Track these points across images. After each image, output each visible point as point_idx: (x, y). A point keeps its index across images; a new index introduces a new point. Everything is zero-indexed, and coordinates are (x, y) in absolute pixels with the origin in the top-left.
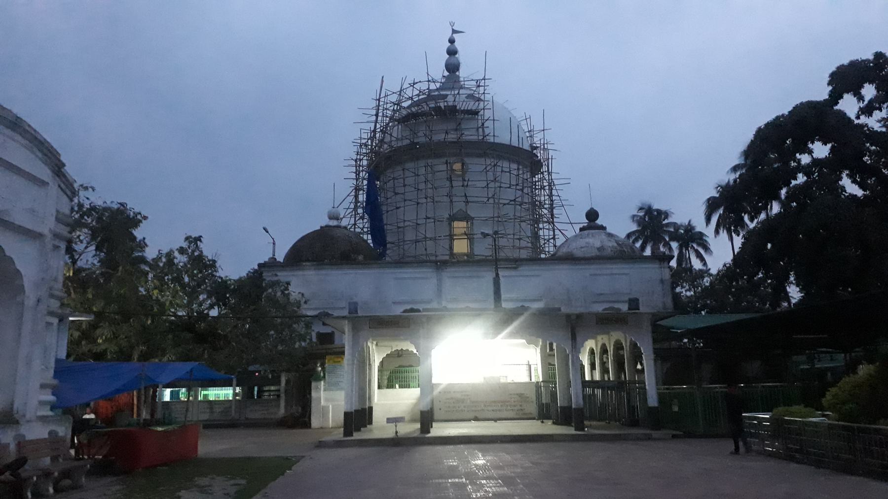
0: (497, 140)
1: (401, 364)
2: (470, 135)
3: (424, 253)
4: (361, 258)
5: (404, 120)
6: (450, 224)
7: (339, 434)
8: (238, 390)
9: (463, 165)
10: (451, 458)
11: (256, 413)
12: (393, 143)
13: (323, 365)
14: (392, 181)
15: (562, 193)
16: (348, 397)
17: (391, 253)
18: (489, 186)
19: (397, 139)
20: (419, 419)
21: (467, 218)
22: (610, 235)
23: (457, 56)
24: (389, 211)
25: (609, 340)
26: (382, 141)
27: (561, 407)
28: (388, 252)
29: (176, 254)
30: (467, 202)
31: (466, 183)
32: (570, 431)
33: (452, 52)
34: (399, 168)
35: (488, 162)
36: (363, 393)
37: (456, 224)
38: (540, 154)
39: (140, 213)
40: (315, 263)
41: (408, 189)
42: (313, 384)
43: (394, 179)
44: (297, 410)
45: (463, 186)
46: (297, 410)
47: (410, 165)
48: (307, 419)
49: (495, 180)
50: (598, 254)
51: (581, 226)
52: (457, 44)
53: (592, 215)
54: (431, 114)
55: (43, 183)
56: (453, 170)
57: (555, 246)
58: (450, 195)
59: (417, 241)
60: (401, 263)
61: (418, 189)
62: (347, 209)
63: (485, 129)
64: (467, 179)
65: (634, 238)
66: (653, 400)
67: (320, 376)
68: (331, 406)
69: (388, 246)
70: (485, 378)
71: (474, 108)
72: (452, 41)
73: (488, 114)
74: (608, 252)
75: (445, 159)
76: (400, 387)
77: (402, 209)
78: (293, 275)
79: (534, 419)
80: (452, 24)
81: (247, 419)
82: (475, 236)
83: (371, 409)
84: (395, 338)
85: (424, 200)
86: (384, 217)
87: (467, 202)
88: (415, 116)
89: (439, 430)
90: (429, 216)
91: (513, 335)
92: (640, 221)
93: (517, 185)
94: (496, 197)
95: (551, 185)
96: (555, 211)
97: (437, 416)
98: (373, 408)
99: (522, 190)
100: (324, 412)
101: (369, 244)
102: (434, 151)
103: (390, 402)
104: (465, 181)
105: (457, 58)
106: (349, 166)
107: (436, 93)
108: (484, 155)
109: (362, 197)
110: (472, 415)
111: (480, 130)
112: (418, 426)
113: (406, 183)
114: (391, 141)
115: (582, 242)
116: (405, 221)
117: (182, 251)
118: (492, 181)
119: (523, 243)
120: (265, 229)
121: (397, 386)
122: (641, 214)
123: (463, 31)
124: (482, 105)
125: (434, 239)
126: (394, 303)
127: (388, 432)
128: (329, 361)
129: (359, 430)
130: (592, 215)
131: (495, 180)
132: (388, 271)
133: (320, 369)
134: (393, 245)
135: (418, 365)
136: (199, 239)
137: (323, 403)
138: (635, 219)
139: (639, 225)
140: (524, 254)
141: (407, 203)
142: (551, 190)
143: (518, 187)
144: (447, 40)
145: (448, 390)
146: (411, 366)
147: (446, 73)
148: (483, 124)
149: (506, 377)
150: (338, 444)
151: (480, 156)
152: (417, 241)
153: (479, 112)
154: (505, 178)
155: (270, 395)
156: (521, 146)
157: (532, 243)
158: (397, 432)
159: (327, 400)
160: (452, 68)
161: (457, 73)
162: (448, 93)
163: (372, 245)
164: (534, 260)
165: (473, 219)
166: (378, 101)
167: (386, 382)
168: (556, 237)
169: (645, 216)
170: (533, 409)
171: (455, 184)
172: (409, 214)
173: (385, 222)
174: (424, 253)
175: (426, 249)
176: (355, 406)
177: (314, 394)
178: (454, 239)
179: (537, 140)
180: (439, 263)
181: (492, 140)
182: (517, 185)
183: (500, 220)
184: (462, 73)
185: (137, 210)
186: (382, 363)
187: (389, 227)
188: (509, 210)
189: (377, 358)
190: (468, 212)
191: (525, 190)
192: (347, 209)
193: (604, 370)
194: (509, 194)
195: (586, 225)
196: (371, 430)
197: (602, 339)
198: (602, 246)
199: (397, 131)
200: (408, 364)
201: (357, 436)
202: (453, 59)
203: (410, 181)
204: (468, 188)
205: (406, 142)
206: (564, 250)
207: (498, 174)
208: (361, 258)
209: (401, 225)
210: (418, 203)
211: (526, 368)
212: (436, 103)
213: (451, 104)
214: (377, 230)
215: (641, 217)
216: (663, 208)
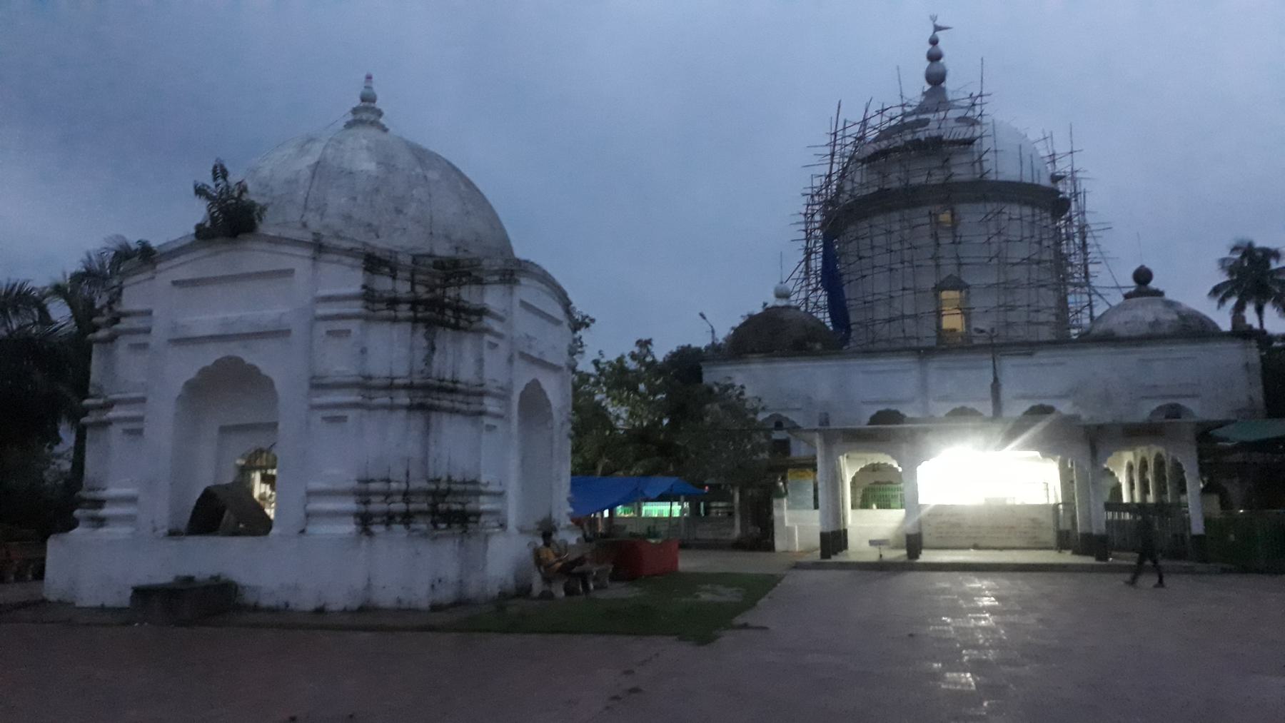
0: (1001, 178)
1: (877, 480)
2: (962, 171)
3: (902, 335)
4: (818, 346)
5: (871, 159)
6: (937, 296)
7: (817, 556)
8: (686, 505)
9: (953, 215)
10: (942, 581)
11: (706, 533)
12: (856, 192)
13: (784, 479)
14: (854, 242)
15: (1100, 243)
16: (824, 520)
17: (857, 335)
18: (991, 241)
19: (861, 185)
20: (905, 544)
21: (958, 285)
22: (1170, 304)
23: (942, 61)
24: (852, 281)
25: (1149, 452)
26: (840, 189)
27: (1082, 534)
28: (853, 334)
29: (628, 359)
30: (960, 265)
31: (958, 240)
32: (1090, 560)
33: (934, 57)
34: (865, 224)
35: (989, 207)
36: (836, 513)
37: (944, 295)
38: (1065, 189)
39: (587, 317)
40: (762, 355)
41: (877, 251)
42: (775, 502)
43: (857, 238)
44: (755, 531)
45: (953, 243)
46: (755, 531)
47: (879, 220)
48: (769, 541)
49: (999, 233)
50: (1150, 331)
51: (1126, 291)
52: (941, 45)
53: (1143, 276)
54: (907, 149)
55: (558, 323)
56: (938, 223)
57: (1092, 317)
58: (935, 258)
59: (890, 320)
60: (869, 352)
61: (892, 251)
62: (798, 279)
63: (985, 164)
64: (958, 234)
65: (1224, 292)
66: (1197, 528)
67: (781, 491)
68: (796, 527)
69: (853, 327)
70: (986, 500)
71: (968, 136)
72: (934, 42)
73: (987, 143)
74: (1165, 329)
75: (929, 208)
76: (878, 508)
77: (870, 277)
78: (737, 370)
79: (1051, 548)
80: (934, 19)
81: (696, 539)
82: (973, 311)
83: (845, 531)
84: (873, 450)
85: (899, 266)
86: (845, 288)
87: (960, 265)
88: (884, 153)
89: (926, 557)
90: (907, 286)
91: (1029, 446)
92: (1232, 268)
93: (1032, 237)
94: (1000, 255)
95: (1083, 229)
96: (1091, 268)
97: (926, 540)
98: (848, 531)
99: (1040, 243)
100: (790, 532)
101: (827, 328)
102: (910, 197)
103: (866, 525)
104: (956, 236)
105: (942, 65)
106: (798, 223)
107: (914, 118)
108: (985, 199)
109: (817, 263)
110: (972, 542)
111: (977, 165)
112: (904, 552)
113: (874, 244)
114: (853, 190)
115: (1124, 316)
116: (874, 294)
117: (633, 356)
118: (995, 235)
119: (1042, 317)
120: (702, 315)
121: (874, 506)
122: (1237, 256)
124: (978, 131)
125: (915, 316)
126: (863, 402)
127: (872, 555)
128: (791, 474)
129: (835, 553)
130: (1143, 276)
131: (999, 233)
132: (852, 362)
133: (781, 484)
134: (858, 326)
135: (901, 481)
136: (649, 342)
137: (787, 524)
138: (1227, 264)
139: (1231, 273)
140: (1045, 334)
141: (876, 270)
142: (1084, 239)
143: (1034, 240)
144: (928, 39)
145: (938, 512)
146: (891, 483)
147: (927, 87)
148: (980, 157)
149: (1014, 498)
150: (815, 566)
151: (977, 200)
152: (890, 320)
153: (974, 141)
154: (1014, 230)
155: (717, 513)
156: (1036, 182)
157: (1057, 316)
158: (881, 556)
159: (791, 520)
160: (936, 79)
161: (943, 85)
162: (930, 116)
163: (831, 328)
164: (1061, 342)
165: (968, 287)
166: (833, 137)
167: (859, 501)
168: (1094, 303)
169: (1242, 257)
170: (1050, 537)
171: (942, 241)
172: (880, 284)
173: (847, 297)
174: (902, 335)
175: (904, 331)
176: (830, 528)
177: (776, 513)
178: (943, 315)
179: (1062, 167)
180: (922, 351)
181: (993, 178)
182: (1032, 237)
183: (1007, 286)
184: (950, 85)
185: (585, 313)
186: (854, 479)
187: (852, 302)
188: (1019, 273)
189: (849, 471)
190: (963, 279)
191: (1045, 243)
192: (798, 279)
193: (1145, 491)
194: (1019, 252)
195: (1133, 289)
196: (847, 555)
197: (1142, 451)
198: (1157, 320)
199: (860, 176)
200: (886, 480)
201: (834, 559)
202: (935, 65)
203: (880, 240)
204: (961, 246)
205: (871, 190)
206: (1100, 328)
207: (1003, 224)
208: (818, 346)
209: (870, 298)
210: (891, 270)
211: (1044, 486)
212: (915, 133)
213: (935, 133)
214: (837, 306)
215: (1236, 262)
216: (1270, 244)
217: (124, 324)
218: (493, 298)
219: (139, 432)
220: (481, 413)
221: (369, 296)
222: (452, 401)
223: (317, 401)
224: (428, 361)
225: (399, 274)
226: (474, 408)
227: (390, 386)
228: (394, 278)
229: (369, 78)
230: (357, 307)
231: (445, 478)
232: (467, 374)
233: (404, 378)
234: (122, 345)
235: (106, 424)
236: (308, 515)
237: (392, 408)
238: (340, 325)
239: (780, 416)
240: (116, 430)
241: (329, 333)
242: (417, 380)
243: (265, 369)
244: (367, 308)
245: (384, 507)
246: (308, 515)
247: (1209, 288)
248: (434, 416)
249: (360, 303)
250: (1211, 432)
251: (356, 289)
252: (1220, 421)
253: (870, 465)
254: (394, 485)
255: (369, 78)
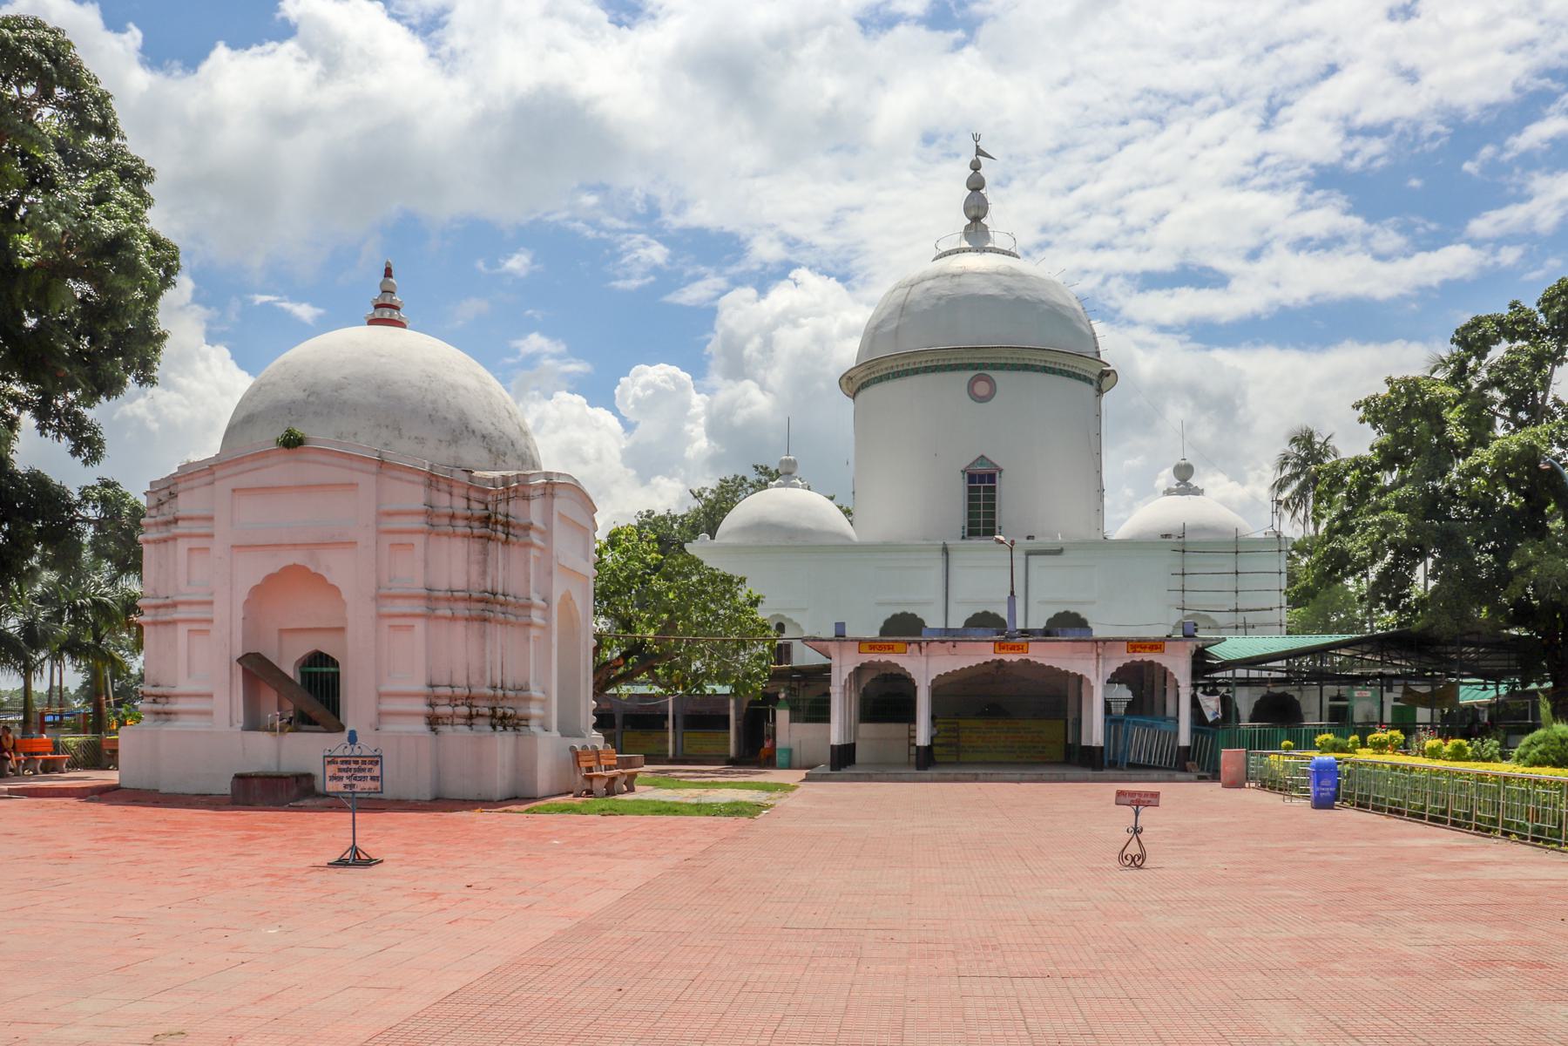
123: (993, 156)
217: (182, 528)
218: (534, 512)
219: (207, 631)
220: (529, 625)
221: (430, 512)
222: (503, 613)
223: (385, 610)
224: (484, 573)
225: (456, 491)
226: (523, 620)
227: (451, 597)
228: (451, 494)
229: (388, 273)
230: (418, 523)
231: (499, 686)
232: (515, 587)
233: (463, 591)
234: (182, 546)
235: (174, 622)
236: (381, 714)
237: (453, 618)
238: (405, 539)
239: (782, 616)
240: (182, 630)
241: (392, 545)
242: (475, 595)
243: (332, 579)
244: (427, 523)
245: (449, 710)
246: (381, 714)
247: (1335, 436)
248: (489, 627)
249: (422, 519)
250: (1207, 649)
251: (419, 505)
252: (99, 801)
253: (883, 674)
254: (458, 691)
255: (388, 273)
